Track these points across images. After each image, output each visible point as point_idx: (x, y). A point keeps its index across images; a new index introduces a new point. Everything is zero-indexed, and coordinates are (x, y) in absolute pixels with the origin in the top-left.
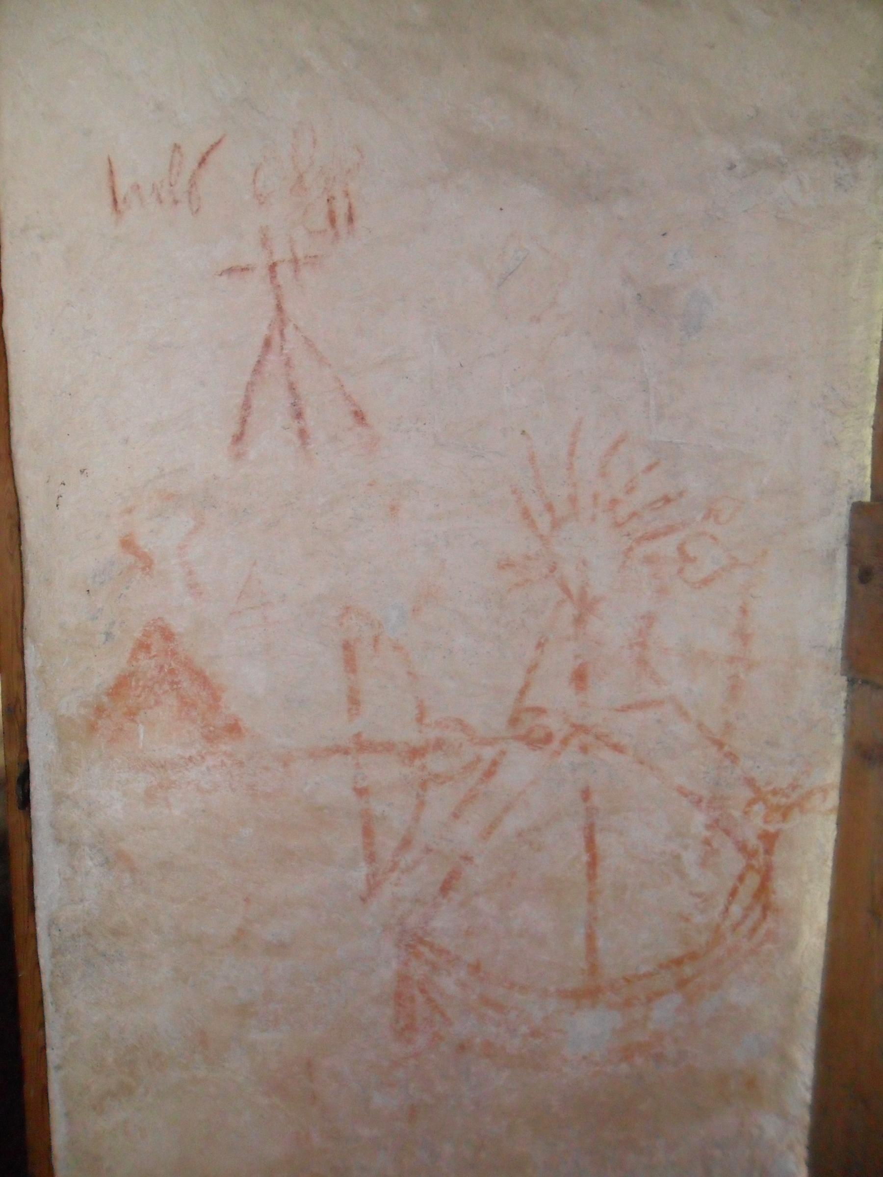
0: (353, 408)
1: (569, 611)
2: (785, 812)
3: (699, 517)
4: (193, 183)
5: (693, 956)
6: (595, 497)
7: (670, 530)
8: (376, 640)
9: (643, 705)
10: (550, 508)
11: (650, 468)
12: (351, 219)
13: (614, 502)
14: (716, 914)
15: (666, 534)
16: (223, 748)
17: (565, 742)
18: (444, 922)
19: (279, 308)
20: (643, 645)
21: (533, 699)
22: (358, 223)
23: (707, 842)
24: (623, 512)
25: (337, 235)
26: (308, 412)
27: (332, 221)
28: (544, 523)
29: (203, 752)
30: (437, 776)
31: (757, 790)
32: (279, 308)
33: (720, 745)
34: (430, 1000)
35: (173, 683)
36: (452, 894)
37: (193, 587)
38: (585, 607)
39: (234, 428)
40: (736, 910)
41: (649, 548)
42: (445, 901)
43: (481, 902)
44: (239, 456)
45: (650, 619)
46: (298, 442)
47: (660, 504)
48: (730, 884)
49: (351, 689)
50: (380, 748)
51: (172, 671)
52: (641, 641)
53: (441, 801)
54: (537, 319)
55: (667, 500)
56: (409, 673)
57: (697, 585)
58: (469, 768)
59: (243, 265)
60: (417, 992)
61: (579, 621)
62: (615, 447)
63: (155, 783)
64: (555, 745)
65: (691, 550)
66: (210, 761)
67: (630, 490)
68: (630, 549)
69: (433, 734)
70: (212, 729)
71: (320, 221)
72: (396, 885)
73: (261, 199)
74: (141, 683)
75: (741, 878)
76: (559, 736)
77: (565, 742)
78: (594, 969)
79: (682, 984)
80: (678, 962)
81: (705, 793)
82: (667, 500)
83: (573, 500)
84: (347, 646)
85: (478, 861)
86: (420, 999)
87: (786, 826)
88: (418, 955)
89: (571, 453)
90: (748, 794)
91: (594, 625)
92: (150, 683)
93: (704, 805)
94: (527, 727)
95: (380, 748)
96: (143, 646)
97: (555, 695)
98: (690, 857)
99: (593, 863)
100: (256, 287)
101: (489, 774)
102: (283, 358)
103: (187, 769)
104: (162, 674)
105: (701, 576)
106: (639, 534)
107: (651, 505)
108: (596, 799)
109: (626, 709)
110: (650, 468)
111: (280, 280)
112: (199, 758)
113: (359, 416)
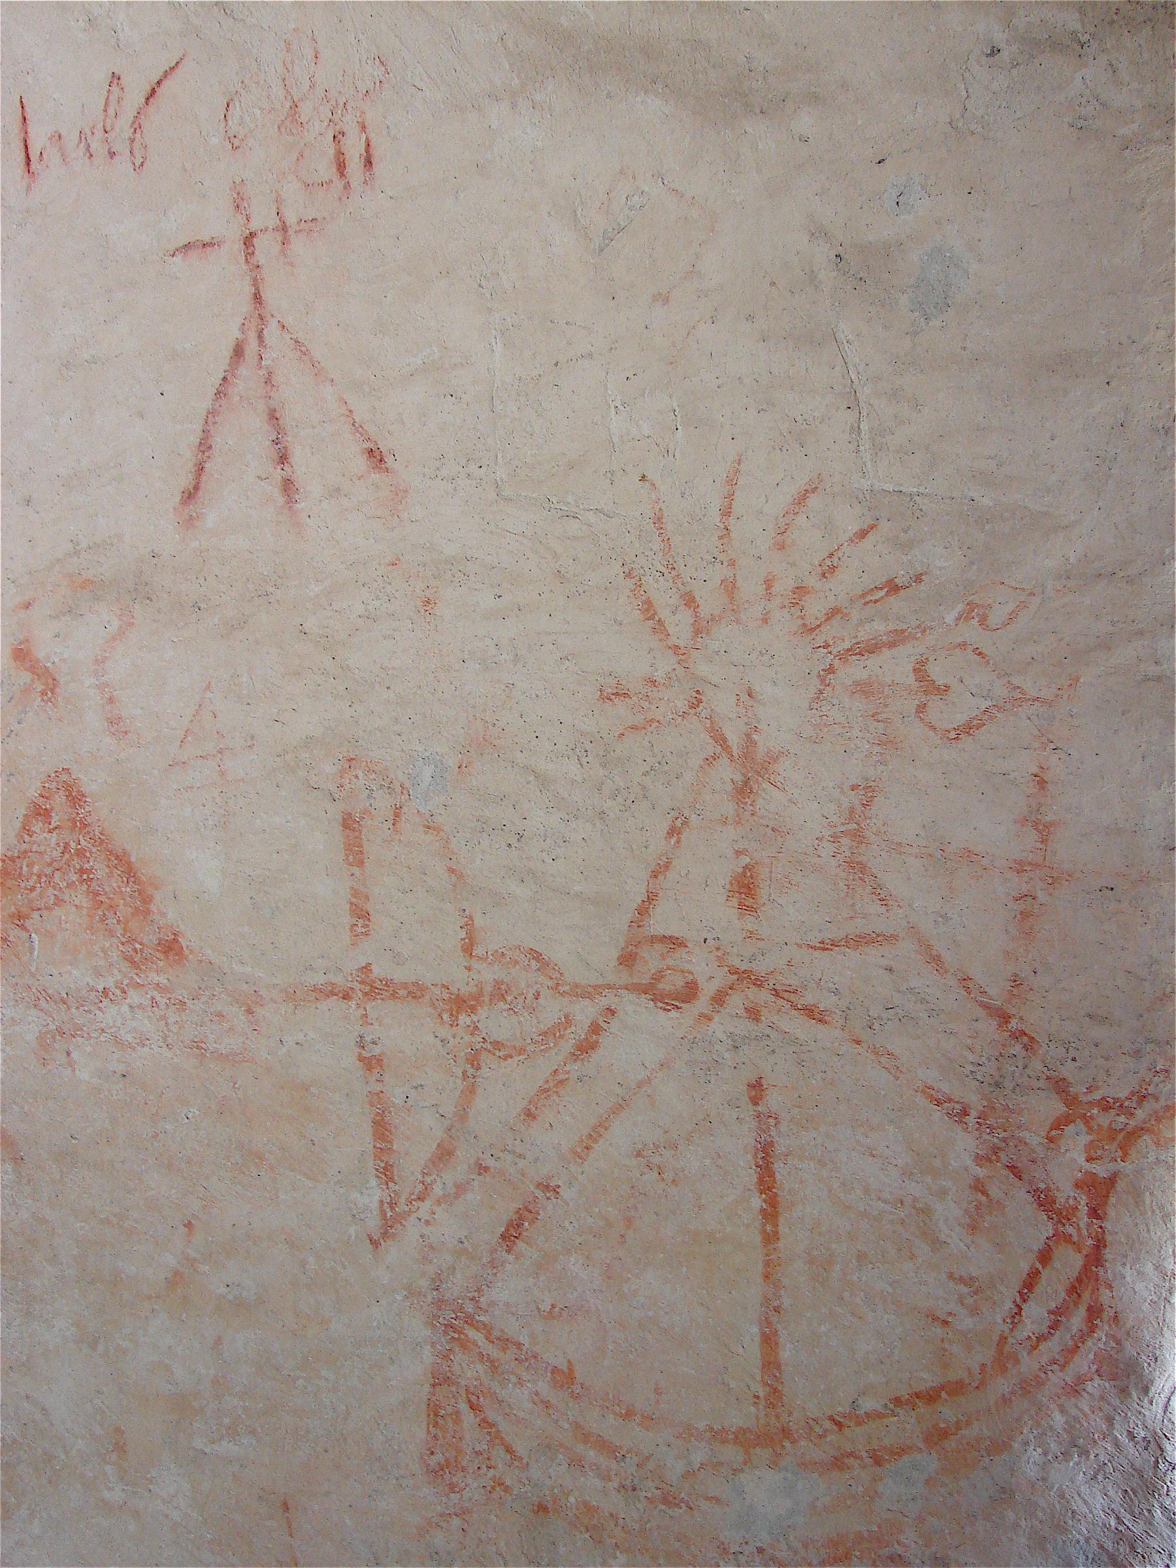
0: (368, 445)
1: (726, 773)
2: (1127, 1139)
3: (950, 618)
4: (137, 127)
5: (957, 1388)
6: (768, 583)
7: (898, 638)
8: (397, 812)
9: (860, 941)
10: (690, 601)
11: (863, 534)
12: (369, 163)
13: (800, 590)
14: (998, 1317)
15: (892, 645)
16: (155, 978)
17: (719, 999)
18: (511, 1291)
19: (257, 298)
20: (858, 836)
21: (661, 922)
22: (378, 168)
23: (979, 1187)
24: (815, 608)
25: (347, 186)
26: (298, 455)
27: (341, 167)
28: (679, 626)
29: (126, 982)
30: (497, 1045)
31: (1071, 1101)
32: (257, 298)
33: (1004, 1018)
34: (486, 1423)
35: (82, 871)
36: (521, 1245)
37: (115, 724)
38: (753, 771)
39: (185, 480)
40: (1036, 1313)
41: (854, 671)
42: (511, 1258)
43: (574, 1263)
44: (190, 523)
45: (868, 792)
46: (281, 500)
47: (882, 593)
48: (1024, 1266)
49: (355, 893)
50: (402, 992)
51: (80, 853)
52: (853, 831)
53: (503, 1091)
54: (663, 299)
55: (893, 588)
56: (451, 870)
57: (953, 735)
58: (552, 1034)
59: (207, 239)
60: (463, 1406)
61: (743, 791)
62: (802, 499)
63: (52, 1027)
64: (702, 1003)
65: (936, 672)
66: (134, 997)
67: (828, 571)
68: (831, 670)
69: (488, 974)
70: (138, 946)
71: (325, 169)
72: (427, 1222)
73: (234, 143)
74: (36, 869)
75: (1045, 1256)
76: (708, 989)
77: (719, 999)
78: (774, 1396)
79: (937, 1436)
80: (931, 1397)
81: (975, 1101)
82: (893, 588)
83: (730, 587)
84: (349, 823)
85: (565, 1193)
86: (469, 1418)
87: (1127, 1167)
88: (464, 1344)
89: (726, 513)
90: (1058, 1108)
91: (770, 800)
92: (48, 871)
93: (971, 1120)
94: (650, 968)
95: (402, 992)
96: (40, 812)
97: (698, 908)
98: (949, 1213)
99: (771, 1212)
100: (223, 272)
101: (586, 1048)
102: (261, 373)
103: (100, 1009)
104: (67, 856)
105: (960, 718)
106: (847, 645)
107: (866, 598)
108: (773, 1100)
109: (825, 947)
110: (863, 534)
111: (260, 257)
112: (118, 992)
113: (376, 457)
